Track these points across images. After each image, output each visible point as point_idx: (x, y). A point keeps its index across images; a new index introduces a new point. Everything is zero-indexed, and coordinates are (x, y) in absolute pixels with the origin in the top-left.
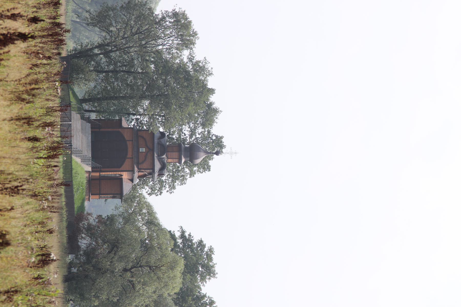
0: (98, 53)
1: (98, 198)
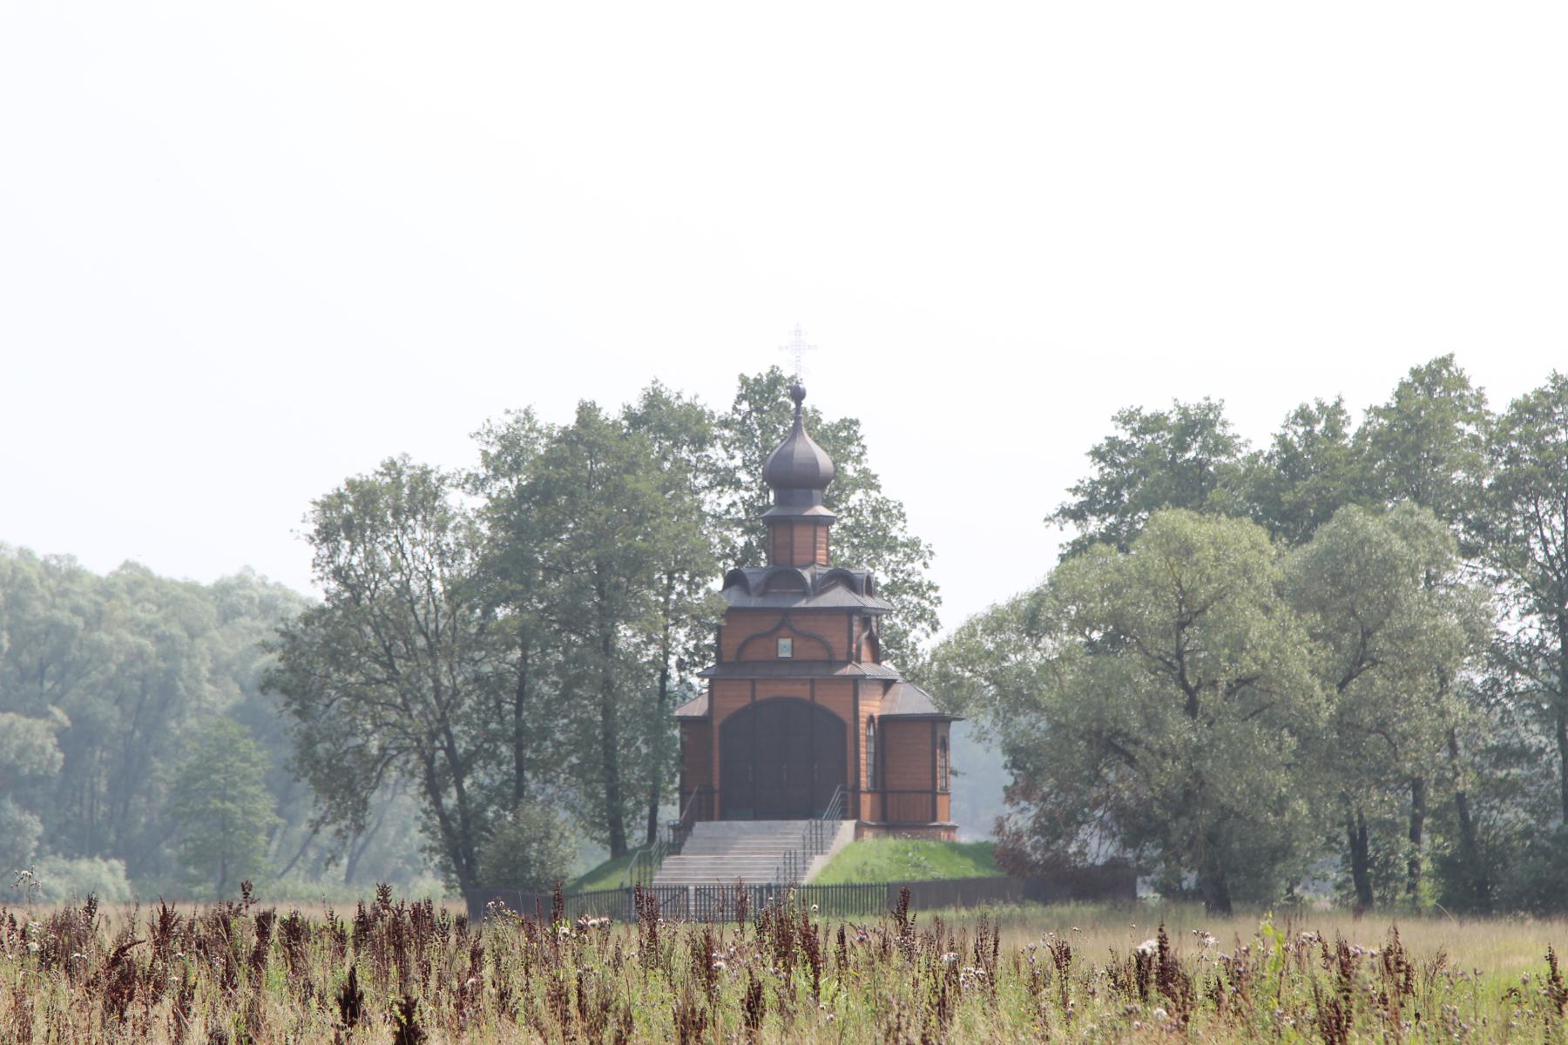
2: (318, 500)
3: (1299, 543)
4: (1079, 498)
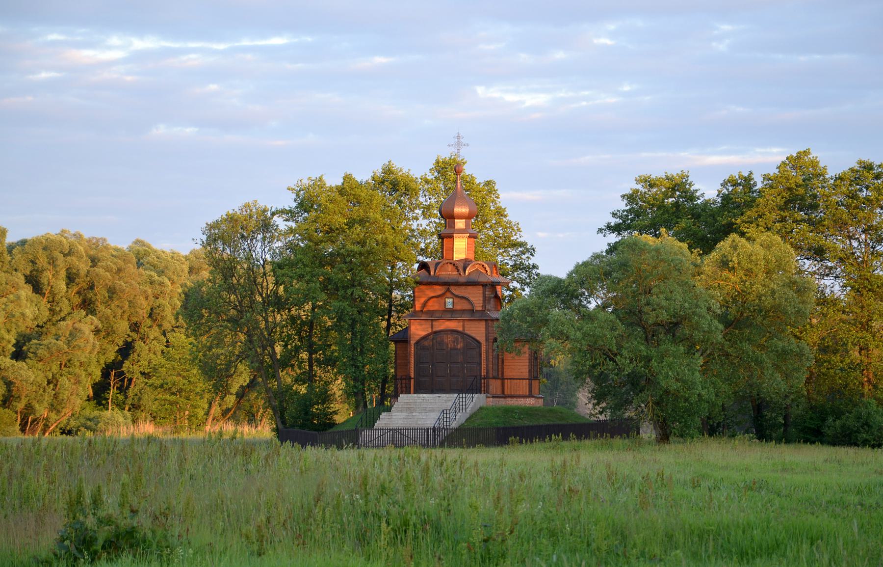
0: (391, 332)
1: (537, 381)
2: (209, 223)
3: (105, 542)
4: (619, 221)
